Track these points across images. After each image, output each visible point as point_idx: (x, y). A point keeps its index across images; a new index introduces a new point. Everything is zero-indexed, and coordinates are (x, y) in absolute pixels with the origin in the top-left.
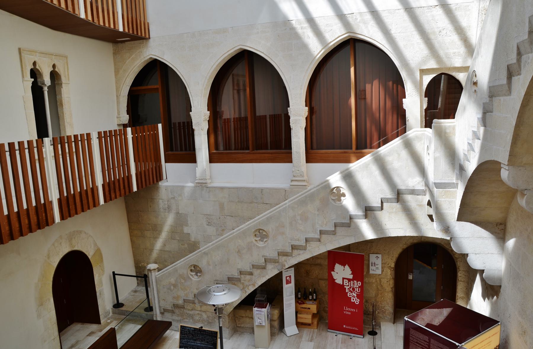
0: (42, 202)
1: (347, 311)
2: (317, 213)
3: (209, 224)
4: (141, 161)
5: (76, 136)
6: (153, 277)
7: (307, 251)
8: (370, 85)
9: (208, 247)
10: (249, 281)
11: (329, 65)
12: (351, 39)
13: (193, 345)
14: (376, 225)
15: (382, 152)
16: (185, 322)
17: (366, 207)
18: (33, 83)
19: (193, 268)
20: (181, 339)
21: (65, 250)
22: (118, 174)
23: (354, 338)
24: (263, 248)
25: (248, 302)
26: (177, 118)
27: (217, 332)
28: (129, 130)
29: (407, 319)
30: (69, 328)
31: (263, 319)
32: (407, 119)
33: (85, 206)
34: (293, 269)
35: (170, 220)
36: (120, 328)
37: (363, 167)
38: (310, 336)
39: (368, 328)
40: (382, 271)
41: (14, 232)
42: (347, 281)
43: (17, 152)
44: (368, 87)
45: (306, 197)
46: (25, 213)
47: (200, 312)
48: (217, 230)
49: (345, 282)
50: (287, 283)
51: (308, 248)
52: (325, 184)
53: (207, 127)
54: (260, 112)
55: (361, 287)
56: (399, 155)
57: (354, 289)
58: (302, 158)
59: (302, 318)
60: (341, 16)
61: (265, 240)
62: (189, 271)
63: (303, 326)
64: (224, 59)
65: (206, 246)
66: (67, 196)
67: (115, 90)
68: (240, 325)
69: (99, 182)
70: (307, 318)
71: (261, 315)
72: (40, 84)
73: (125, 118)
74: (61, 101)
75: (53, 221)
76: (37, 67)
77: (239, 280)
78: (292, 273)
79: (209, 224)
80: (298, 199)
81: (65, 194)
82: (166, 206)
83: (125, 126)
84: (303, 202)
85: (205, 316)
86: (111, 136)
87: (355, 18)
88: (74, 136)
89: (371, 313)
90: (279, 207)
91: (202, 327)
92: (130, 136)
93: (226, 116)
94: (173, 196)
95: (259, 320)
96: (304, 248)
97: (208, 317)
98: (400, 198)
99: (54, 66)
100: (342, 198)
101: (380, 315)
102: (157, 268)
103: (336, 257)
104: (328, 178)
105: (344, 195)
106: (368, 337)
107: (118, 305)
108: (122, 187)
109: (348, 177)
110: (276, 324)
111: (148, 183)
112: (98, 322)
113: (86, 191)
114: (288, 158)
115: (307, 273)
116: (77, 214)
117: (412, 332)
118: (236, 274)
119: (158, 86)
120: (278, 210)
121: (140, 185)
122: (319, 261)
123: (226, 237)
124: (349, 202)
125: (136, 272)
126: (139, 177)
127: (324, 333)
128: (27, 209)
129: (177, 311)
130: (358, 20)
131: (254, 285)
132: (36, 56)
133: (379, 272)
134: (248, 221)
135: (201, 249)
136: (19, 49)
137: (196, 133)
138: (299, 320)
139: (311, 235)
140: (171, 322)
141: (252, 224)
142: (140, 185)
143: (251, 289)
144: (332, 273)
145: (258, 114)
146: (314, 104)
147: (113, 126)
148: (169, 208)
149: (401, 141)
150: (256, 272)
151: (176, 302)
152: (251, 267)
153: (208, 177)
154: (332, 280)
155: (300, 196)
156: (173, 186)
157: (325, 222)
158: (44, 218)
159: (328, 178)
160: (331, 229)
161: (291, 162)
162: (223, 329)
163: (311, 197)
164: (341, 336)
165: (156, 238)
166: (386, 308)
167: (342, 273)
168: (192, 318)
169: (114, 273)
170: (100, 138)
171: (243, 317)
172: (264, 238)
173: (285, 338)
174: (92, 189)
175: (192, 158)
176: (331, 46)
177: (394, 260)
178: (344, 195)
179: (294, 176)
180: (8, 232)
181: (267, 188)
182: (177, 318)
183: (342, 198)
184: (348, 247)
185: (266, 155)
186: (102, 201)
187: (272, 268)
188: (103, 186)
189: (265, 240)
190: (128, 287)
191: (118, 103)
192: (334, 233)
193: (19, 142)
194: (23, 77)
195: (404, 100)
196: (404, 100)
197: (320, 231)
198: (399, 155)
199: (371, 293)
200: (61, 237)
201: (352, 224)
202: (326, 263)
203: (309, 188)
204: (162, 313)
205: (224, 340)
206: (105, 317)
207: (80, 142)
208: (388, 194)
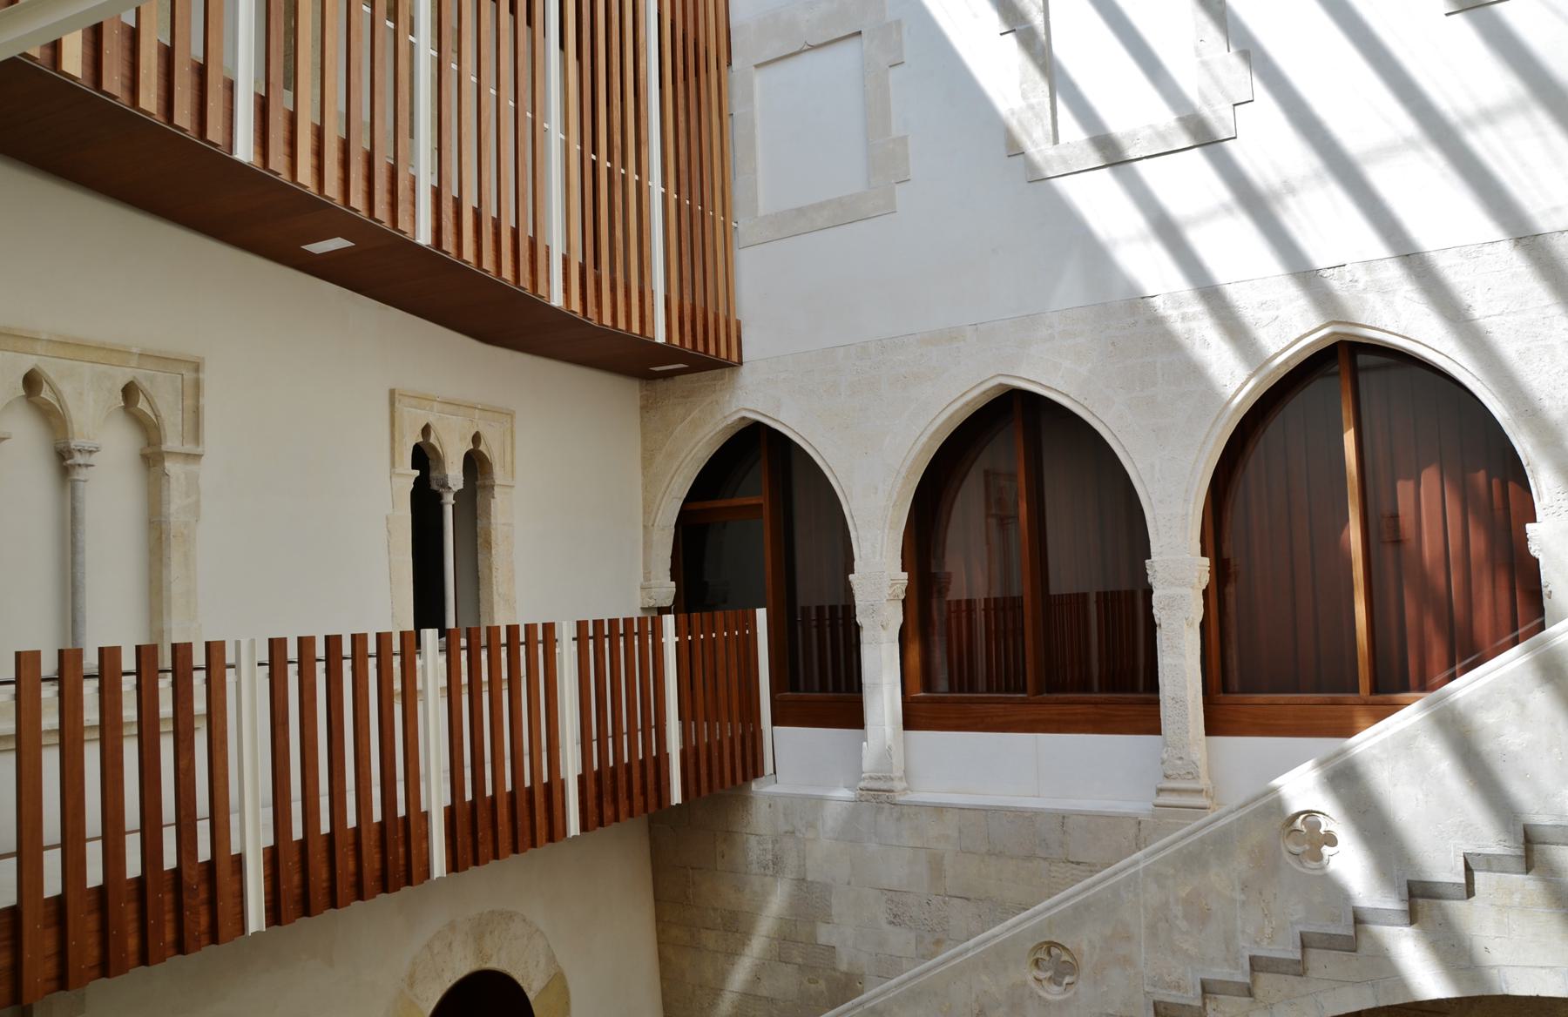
0: (401, 812)
2: (1239, 896)
4: (701, 716)
5: (512, 630)
11: (1273, 431)
12: (1341, 342)
14: (1452, 950)
15: (1459, 695)
18: (417, 481)
21: (461, 966)
24: (1061, 1005)
26: (809, 595)
28: (669, 621)
32: (1545, 591)
33: (524, 838)
43: (347, 665)
44: (1404, 489)
45: (1202, 841)
46: (351, 840)
52: (1264, 801)
53: (900, 620)
54: (1063, 581)
56: (1522, 705)
58: (1191, 718)
60: (1306, 276)
64: (951, 417)
65: (878, 990)
66: (473, 803)
67: (641, 511)
69: (571, 768)
72: (435, 487)
73: (665, 591)
74: (488, 534)
75: (427, 873)
76: (432, 440)
80: (1176, 847)
81: (469, 797)
82: (769, 857)
83: (663, 611)
84: (1192, 859)
87: (1348, 277)
88: (508, 627)
90: (1115, 874)
92: (670, 639)
94: (790, 829)
98: (1536, 857)
99: (476, 438)
100: (1326, 850)
104: (1276, 782)
105: (1331, 840)
108: (636, 789)
109: (1346, 781)
111: (716, 781)
113: (531, 790)
114: (1146, 719)
116: (496, 856)
119: (761, 498)
120: (1111, 881)
121: (692, 788)
124: (1349, 863)
126: (691, 761)
130: (1361, 286)
132: (431, 409)
135: (864, 997)
136: (392, 392)
137: (865, 636)
139: (1219, 973)
141: (1026, 926)
142: (692, 788)
145: (1053, 591)
146: (1228, 551)
147: (629, 607)
148: (777, 861)
149: (1524, 659)
153: (898, 773)
155: (1183, 838)
156: (793, 797)
157: (1268, 931)
158: (402, 862)
159: (1276, 782)
160: (1290, 956)
161: (1157, 730)
163: (1221, 843)
165: (733, 954)
170: (581, 639)
172: (1064, 975)
174: (548, 788)
175: (850, 714)
176: (1279, 367)
178: (1331, 840)
179: (1167, 777)
180: (297, 891)
181: (1079, 814)
183: (1326, 850)
185: (1079, 709)
186: (574, 827)
188: (582, 780)
189: (1067, 979)
191: (647, 545)
192: (1299, 969)
194: (393, 464)
195: (1529, 527)
196: (1529, 527)
197: (1252, 959)
198: (1522, 705)
200: (452, 926)
201: (1364, 943)
203: (1211, 816)
207: (523, 648)
208: (1490, 840)
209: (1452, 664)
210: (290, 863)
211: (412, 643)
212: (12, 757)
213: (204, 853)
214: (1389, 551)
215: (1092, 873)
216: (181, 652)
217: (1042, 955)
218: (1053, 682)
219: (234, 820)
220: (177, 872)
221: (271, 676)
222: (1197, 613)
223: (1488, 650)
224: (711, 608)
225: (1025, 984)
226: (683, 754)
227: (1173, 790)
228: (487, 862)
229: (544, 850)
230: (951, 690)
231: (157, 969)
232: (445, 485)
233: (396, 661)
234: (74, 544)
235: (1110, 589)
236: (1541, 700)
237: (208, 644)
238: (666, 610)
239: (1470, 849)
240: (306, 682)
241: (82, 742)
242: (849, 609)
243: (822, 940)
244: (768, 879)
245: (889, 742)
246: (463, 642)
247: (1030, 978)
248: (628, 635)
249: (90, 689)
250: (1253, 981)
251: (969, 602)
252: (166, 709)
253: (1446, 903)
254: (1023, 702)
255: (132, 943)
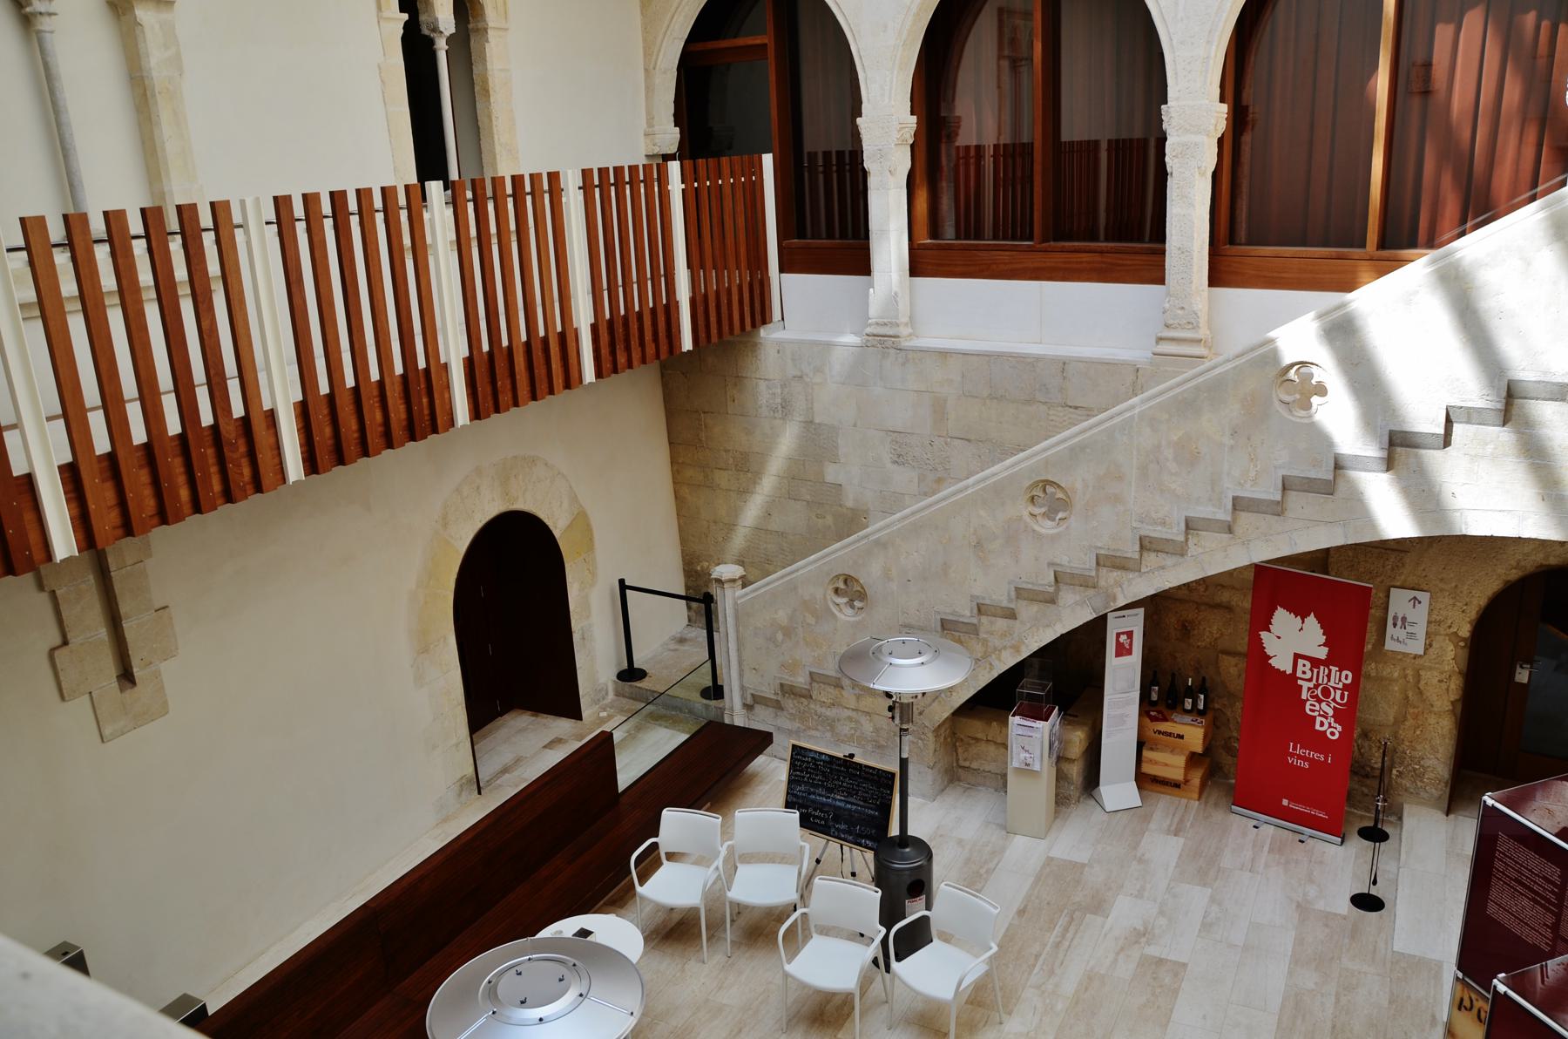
0: (422, 364)
1: (1299, 757)
2: (1228, 441)
3: (899, 460)
4: (709, 263)
5: (517, 180)
6: (728, 601)
7: (1187, 558)
8: (1450, 29)
9: (888, 526)
10: (1003, 635)
13: (823, 804)
16: (811, 737)
17: (1392, 434)
18: (407, 26)
19: (842, 586)
20: (791, 782)
22: (640, 300)
23: (1311, 841)
24: (1054, 539)
25: (997, 699)
26: (817, 139)
27: (893, 775)
28: (674, 168)
29: (1490, 802)
30: (500, 721)
31: (1038, 753)
33: (542, 385)
34: (1141, 611)
35: (786, 443)
36: (631, 737)
37: (1399, 307)
38: (1176, 820)
39: (1362, 817)
40: (1428, 646)
41: (344, 445)
42: (1308, 664)
43: (354, 221)
44: (1443, 33)
45: (1197, 388)
46: (375, 392)
47: (854, 714)
48: (922, 479)
49: (1300, 669)
50: (1118, 655)
51: (1193, 550)
54: (1074, 128)
55: (1352, 689)
57: (1326, 692)
58: (1195, 268)
59: (1156, 763)
61: (1060, 515)
62: (830, 593)
63: (1162, 788)
65: (882, 523)
67: (641, 45)
68: (967, 764)
70: (1171, 764)
71: (1030, 740)
72: (426, 31)
73: (669, 137)
74: (485, 81)
75: (451, 422)
77: (974, 630)
78: (1135, 622)
79: (899, 460)
80: (1171, 394)
81: (486, 347)
83: (667, 158)
84: (1186, 406)
85: (868, 727)
86: (619, 184)
89: (1377, 773)
91: (852, 756)
92: (676, 186)
93: (967, 136)
95: (1023, 755)
96: (1180, 550)
97: (877, 730)
98: (1515, 411)
100: (1315, 400)
101: (1406, 782)
102: (742, 577)
103: (1278, 585)
104: (1272, 334)
105: (1321, 390)
106: (1357, 845)
107: (630, 674)
109: (1343, 334)
110: (1075, 771)
111: (726, 328)
112: (575, 713)
113: (545, 340)
114: (1156, 275)
115: (1186, 629)
117: (1505, 844)
118: (966, 613)
119: (765, 39)
121: (702, 335)
122: (1225, 596)
123: (944, 499)
125: (687, 588)
126: (700, 310)
127: (1219, 816)
128: (381, 383)
129: (789, 703)
131: (1017, 649)
133: (1417, 647)
134: (1013, 454)
137: (872, 182)
138: (1146, 768)
140: (770, 735)
142: (702, 335)
143: (1008, 661)
144: (1263, 634)
145: (1065, 136)
146: (1248, 96)
147: (633, 154)
148: (785, 408)
149: (1541, 215)
150: (1027, 611)
151: (788, 679)
152: (1013, 594)
154: (1258, 656)
155: (1179, 385)
156: (802, 342)
157: (1252, 474)
158: (426, 412)
161: (1161, 280)
162: (911, 768)
163: (1215, 391)
164: (1270, 830)
165: (745, 492)
166: (1427, 763)
167: (1293, 639)
168: (832, 728)
169: (622, 582)
170: (586, 187)
171: (977, 740)
172: (1057, 512)
173: (1098, 816)
174: (562, 337)
175: (857, 261)
177: (1473, 613)
178: (1321, 390)
179: (1167, 326)
180: (330, 442)
181: (1079, 360)
182: (787, 724)
183: (1315, 400)
184: (1322, 559)
185: (1085, 257)
186: (589, 374)
187: (1076, 603)
188: (595, 328)
189: (1060, 515)
190: (662, 630)
191: (649, 89)
192: (1277, 509)
193: (358, 191)
194: (379, 8)
197: (1235, 499)
199: (1382, 711)
201: (1341, 486)
202: (1247, 604)
203: (1208, 364)
204: (748, 707)
205: (911, 800)
206: (596, 702)
207: (529, 198)
208: (1473, 391)
209: (1463, 221)
210: (320, 416)
211: (417, 197)
212: (39, 323)
213: (238, 410)
214: (1416, 102)
215: (1089, 416)
216: (186, 213)
217: (1038, 492)
218: (1060, 230)
219: (262, 378)
220: (215, 428)
221: (280, 234)
222: (1211, 162)
223: (1502, 207)
224: (718, 154)
225: (1020, 518)
226: (693, 302)
227: (1173, 339)
228: (507, 409)
229: (562, 398)
230: (957, 238)
231: (209, 517)
232: (435, 29)
233: (404, 215)
234: (54, 103)
235: (1124, 135)
236: (1547, 258)
237: (212, 204)
238: (671, 157)
239: (1455, 401)
240: (316, 239)
241: (104, 307)
242: (857, 154)
243: (829, 478)
244: (778, 422)
245: (895, 289)
246: (469, 195)
247: (1025, 514)
248: (633, 183)
249: (102, 253)
250: (1234, 520)
251: (978, 148)
252: (181, 273)
253: (1423, 452)
254: (1030, 249)
255: (184, 494)
